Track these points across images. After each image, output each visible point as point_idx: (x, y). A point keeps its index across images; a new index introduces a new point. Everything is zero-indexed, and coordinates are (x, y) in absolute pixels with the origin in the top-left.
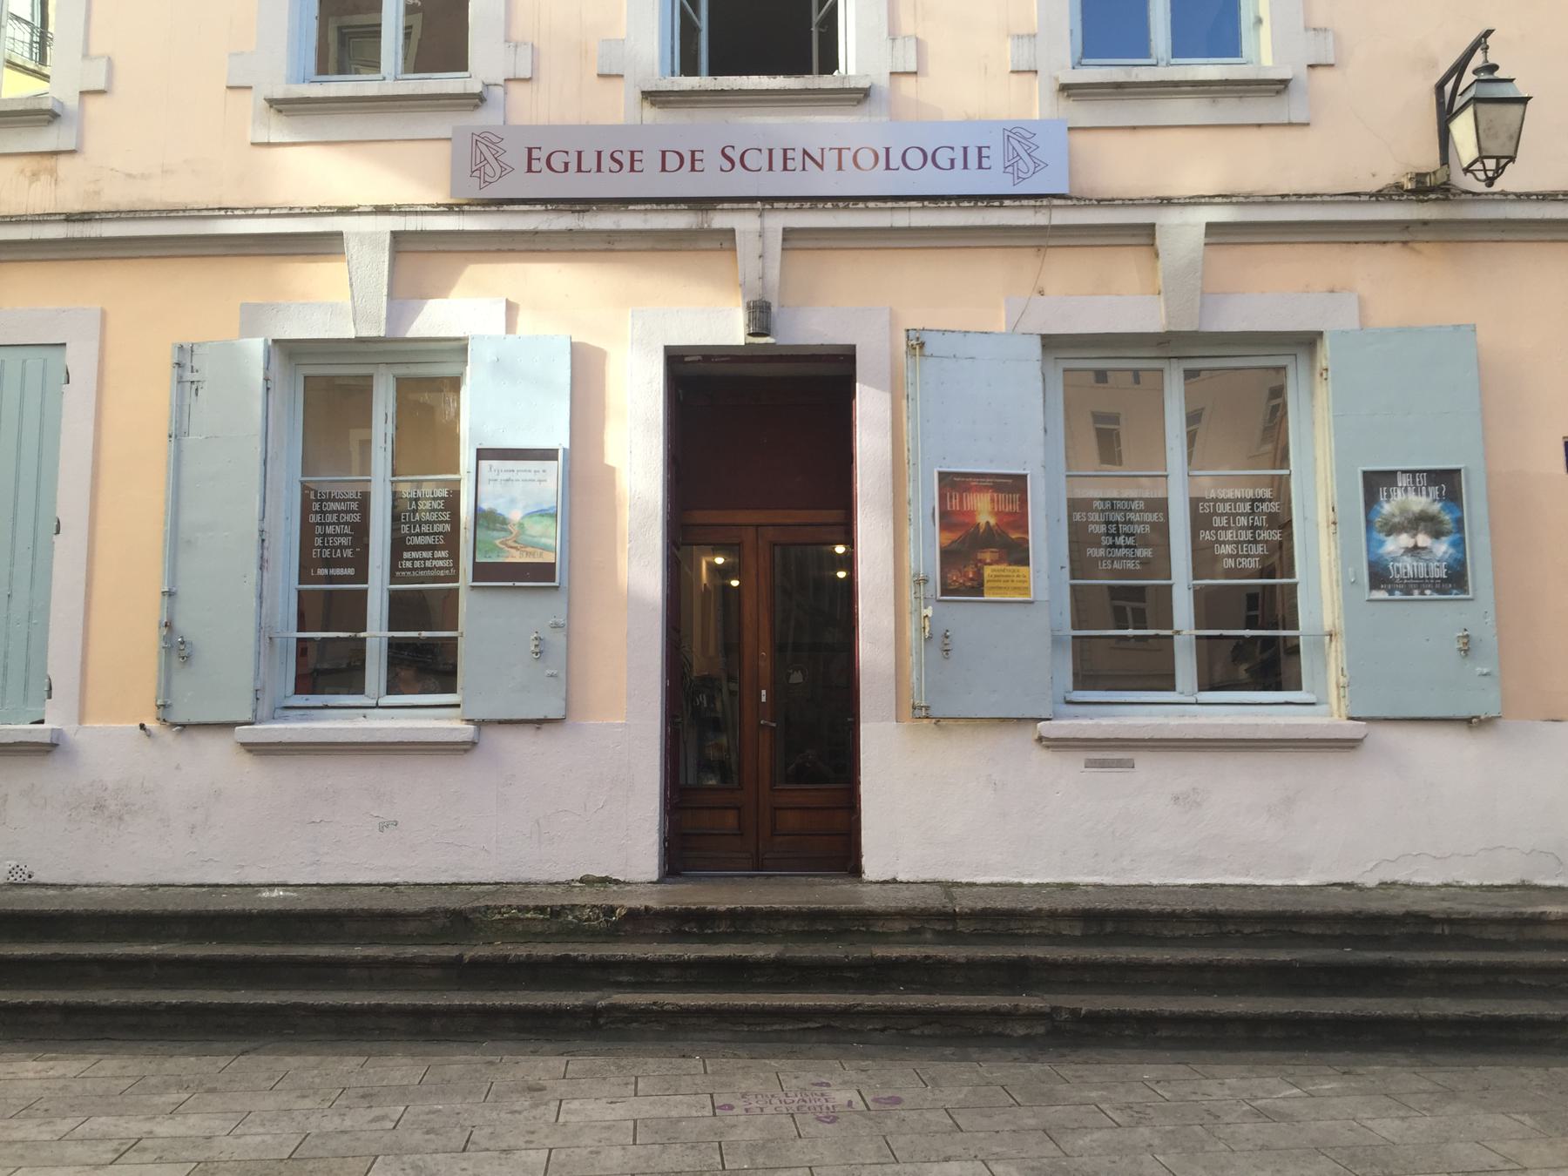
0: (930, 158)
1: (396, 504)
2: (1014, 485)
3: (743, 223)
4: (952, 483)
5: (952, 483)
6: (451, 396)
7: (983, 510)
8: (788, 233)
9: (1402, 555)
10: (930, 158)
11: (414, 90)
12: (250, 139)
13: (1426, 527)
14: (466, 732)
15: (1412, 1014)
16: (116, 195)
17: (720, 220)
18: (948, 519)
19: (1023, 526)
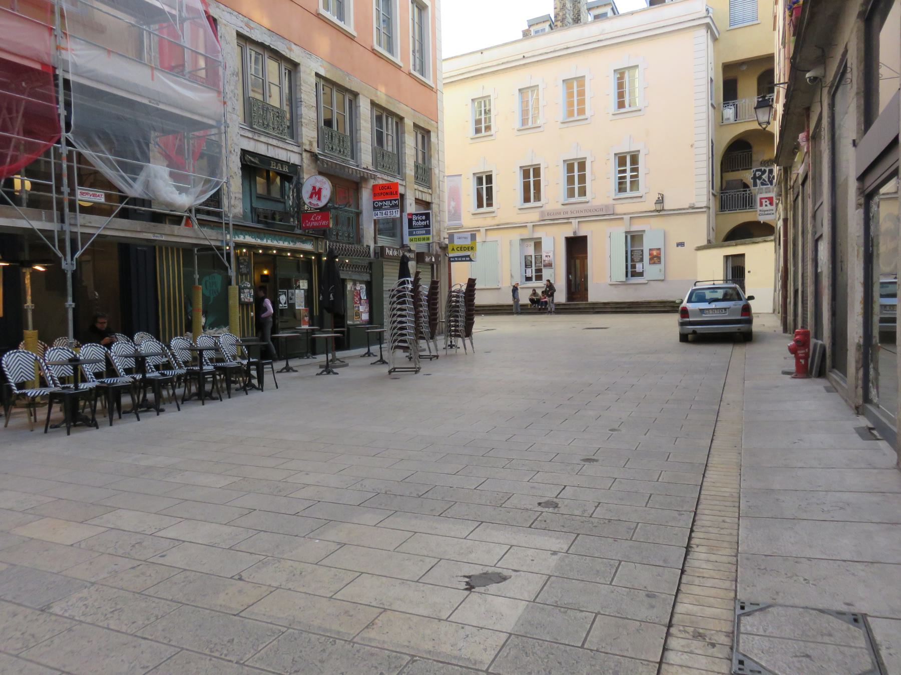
0: (596, 210)
1: (888, 308)
2: (659, 249)
3: (573, 220)
4: (650, 250)
5: (650, 250)
6: (165, 164)
7: (655, 253)
8: (579, 222)
9: (62, 228)
10: (596, 210)
11: (821, 259)
12: (592, 231)
13: (169, 220)
14: (646, 282)
15: (306, 145)
16: (502, 222)
17: (570, 221)
18: (650, 254)
19: (660, 254)
